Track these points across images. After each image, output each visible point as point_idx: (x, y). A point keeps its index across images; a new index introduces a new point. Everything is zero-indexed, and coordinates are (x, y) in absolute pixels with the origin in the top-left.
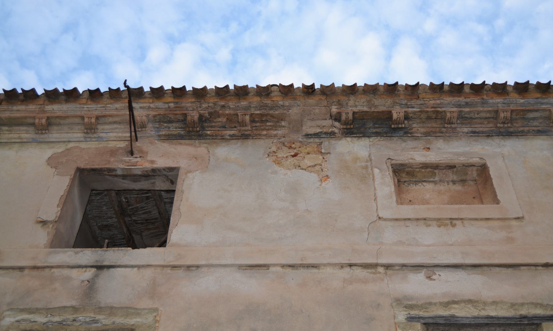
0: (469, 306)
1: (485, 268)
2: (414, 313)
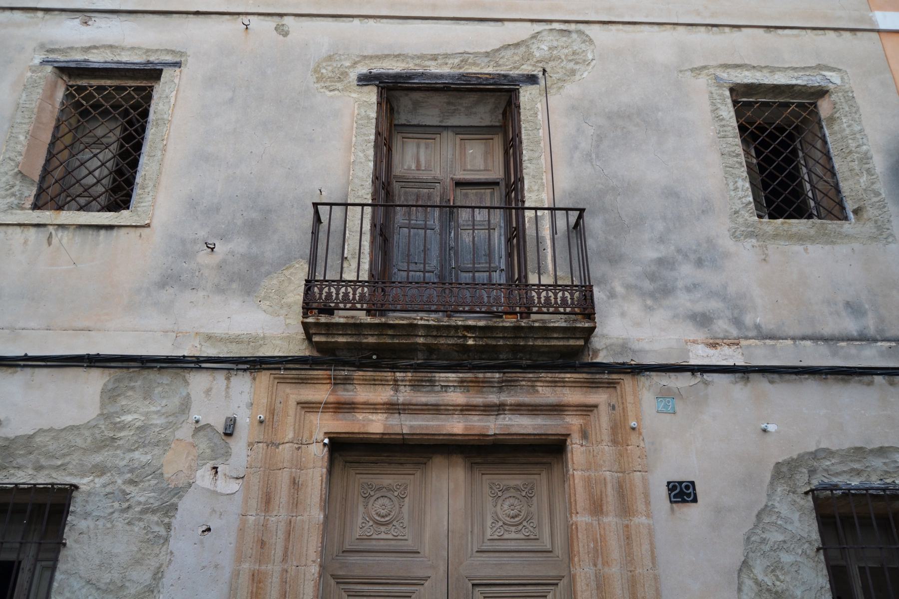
0: (108, 51)
1: (140, 15)
2: (790, 66)
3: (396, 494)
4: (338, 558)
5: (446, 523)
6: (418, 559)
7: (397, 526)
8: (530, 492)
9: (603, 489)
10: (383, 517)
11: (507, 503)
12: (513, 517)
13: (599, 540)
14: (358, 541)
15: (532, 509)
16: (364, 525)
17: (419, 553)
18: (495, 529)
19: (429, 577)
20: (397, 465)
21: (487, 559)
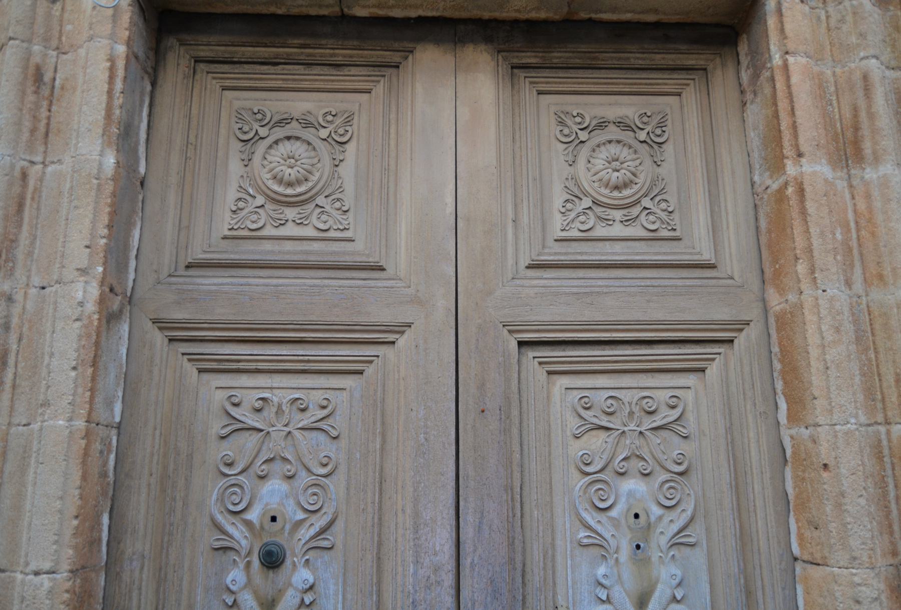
3: (324, 133)
4: (173, 279)
5: (450, 200)
6: (379, 284)
7: (328, 208)
8: (658, 131)
9: (862, 103)
10: (290, 184)
11: (604, 153)
12: (617, 188)
13: (852, 225)
14: (226, 242)
15: (663, 171)
16: (241, 204)
17: (382, 269)
18: (573, 215)
19: (409, 326)
20: (326, 68)
21: (553, 283)
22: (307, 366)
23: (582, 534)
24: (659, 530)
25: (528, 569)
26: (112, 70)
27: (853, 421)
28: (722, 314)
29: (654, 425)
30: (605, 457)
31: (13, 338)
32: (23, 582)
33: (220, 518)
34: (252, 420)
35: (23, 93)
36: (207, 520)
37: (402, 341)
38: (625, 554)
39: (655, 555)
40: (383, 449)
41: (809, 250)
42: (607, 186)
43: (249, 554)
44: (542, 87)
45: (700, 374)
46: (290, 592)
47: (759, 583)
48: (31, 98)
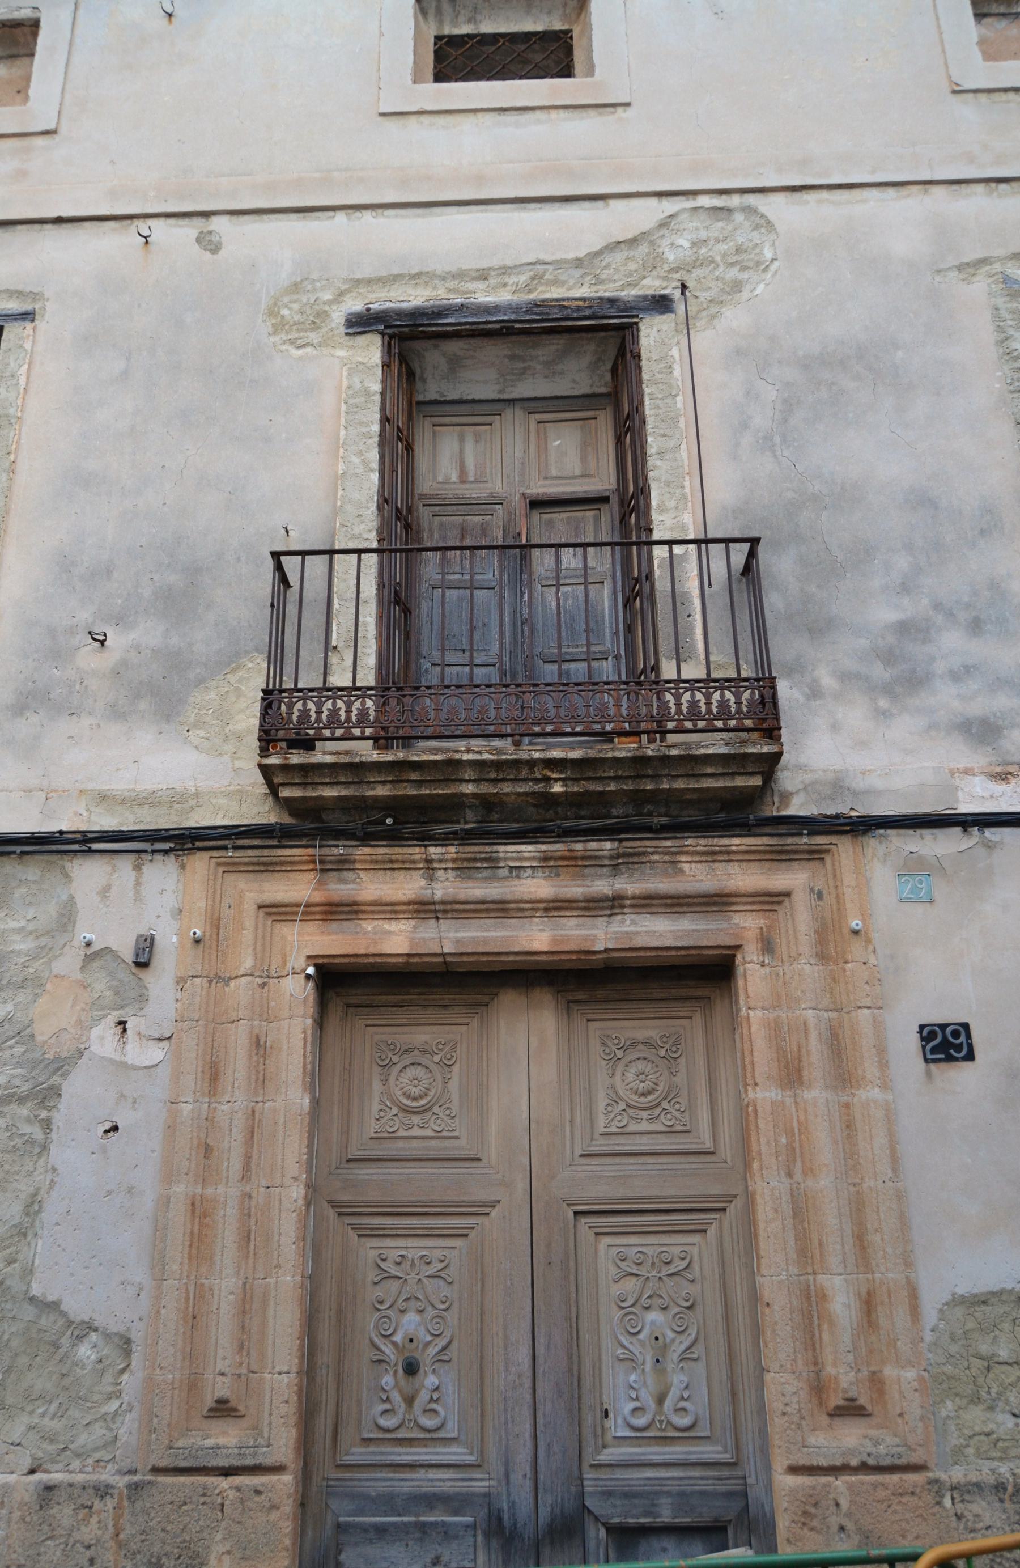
3: (437, 1058)
4: (339, 1171)
5: (525, 1108)
6: (478, 1171)
7: (441, 1115)
10: (415, 1099)
11: (633, 1070)
12: (643, 1095)
13: (796, 1131)
16: (382, 1114)
17: (479, 1160)
18: (612, 1115)
20: (436, 1008)
22: (431, 1232)
23: (620, 1351)
24: (673, 1348)
25: (582, 1376)
26: (305, 1039)
27: (784, 1273)
28: (716, 1190)
29: (670, 1272)
30: (635, 1296)
31: (253, 1222)
32: (272, 1379)
33: (376, 1340)
34: (395, 1271)
35: (250, 1055)
36: (367, 1341)
37: (494, 1213)
38: (648, 1366)
39: (670, 1366)
40: (482, 1290)
41: (760, 1153)
42: (636, 1093)
43: (396, 1365)
44: (589, 1017)
45: (703, 1234)
46: (423, 1392)
47: (741, 1387)
48: (255, 1058)
